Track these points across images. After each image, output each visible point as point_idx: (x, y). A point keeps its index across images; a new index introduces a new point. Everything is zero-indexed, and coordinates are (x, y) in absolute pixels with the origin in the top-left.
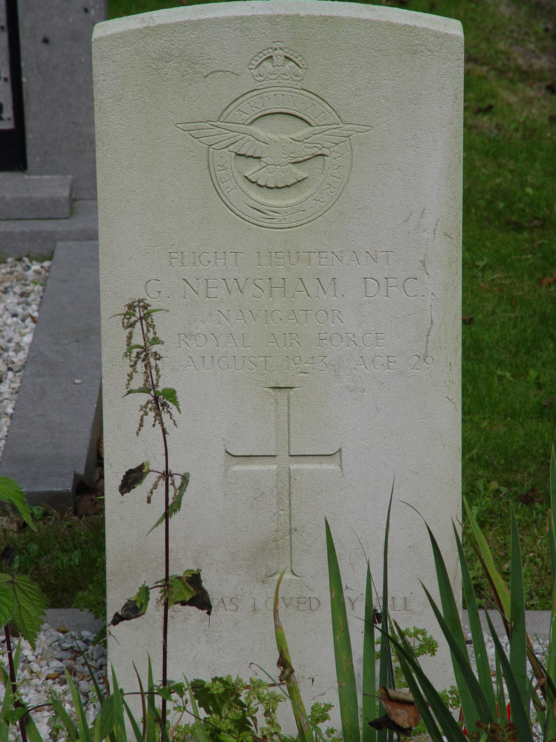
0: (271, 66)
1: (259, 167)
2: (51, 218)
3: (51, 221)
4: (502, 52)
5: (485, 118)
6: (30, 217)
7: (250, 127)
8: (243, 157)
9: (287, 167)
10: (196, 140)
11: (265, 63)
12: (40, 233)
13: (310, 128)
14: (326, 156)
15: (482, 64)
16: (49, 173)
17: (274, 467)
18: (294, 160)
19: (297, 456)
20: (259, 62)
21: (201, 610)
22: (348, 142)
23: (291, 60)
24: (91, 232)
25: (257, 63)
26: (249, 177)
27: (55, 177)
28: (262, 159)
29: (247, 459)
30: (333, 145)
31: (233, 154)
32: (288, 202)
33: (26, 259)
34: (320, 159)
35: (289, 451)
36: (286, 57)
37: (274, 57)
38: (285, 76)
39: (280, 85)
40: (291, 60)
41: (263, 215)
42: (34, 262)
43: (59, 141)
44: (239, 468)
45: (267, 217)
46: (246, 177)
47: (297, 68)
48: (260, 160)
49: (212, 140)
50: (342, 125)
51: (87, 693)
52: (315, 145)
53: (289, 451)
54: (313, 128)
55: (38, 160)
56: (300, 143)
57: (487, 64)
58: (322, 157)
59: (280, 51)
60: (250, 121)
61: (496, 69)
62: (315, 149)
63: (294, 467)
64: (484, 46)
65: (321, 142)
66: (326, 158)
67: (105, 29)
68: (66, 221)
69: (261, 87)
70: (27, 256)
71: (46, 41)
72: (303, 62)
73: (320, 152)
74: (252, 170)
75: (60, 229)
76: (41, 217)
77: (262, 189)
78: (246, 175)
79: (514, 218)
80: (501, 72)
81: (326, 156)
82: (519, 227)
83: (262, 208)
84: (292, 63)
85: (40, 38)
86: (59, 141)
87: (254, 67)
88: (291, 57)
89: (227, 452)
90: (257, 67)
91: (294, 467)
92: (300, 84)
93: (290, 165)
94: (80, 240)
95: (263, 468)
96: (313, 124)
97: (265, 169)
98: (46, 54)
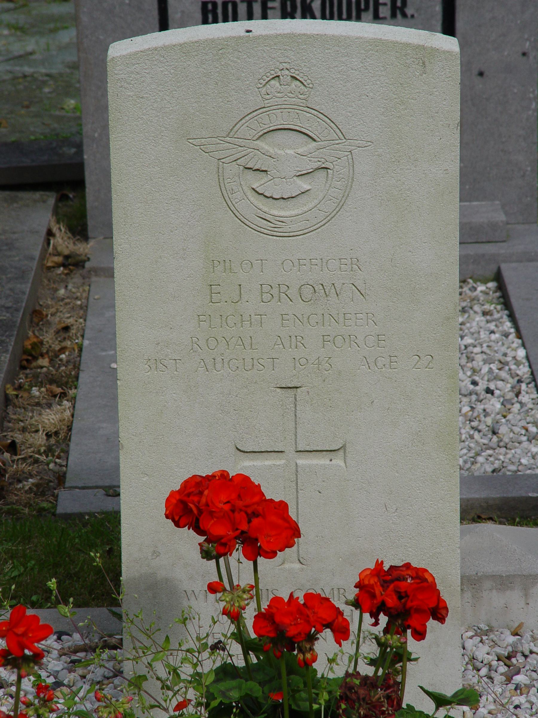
2: (489, 242)
3: (490, 244)
6: (470, 241)
7: (258, 142)
8: (258, 172)
9: (292, 180)
10: (207, 154)
11: (273, 82)
12: (484, 255)
13: (314, 144)
14: (329, 169)
16: (477, 200)
19: (302, 451)
20: (267, 81)
21: (341, 609)
22: (350, 157)
23: (297, 79)
24: (533, 254)
27: (483, 203)
28: (268, 173)
30: (337, 159)
31: (242, 168)
32: (293, 213)
33: (470, 281)
34: (323, 173)
35: (296, 448)
37: (281, 77)
40: (297, 79)
42: (479, 283)
43: (488, 169)
46: (253, 189)
47: (303, 87)
49: (221, 154)
52: (319, 159)
53: (296, 448)
54: (317, 143)
55: (467, 187)
59: (287, 72)
60: (257, 136)
62: (318, 163)
63: (300, 462)
65: (323, 156)
68: (504, 244)
69: (268, 105)
70: (471, 278)
71: (481, 74)
72: (309, 81)
73: (323, 166)
74: (257, 182)
75: (502, 251)
76: (479, 240)
77: (268, 200)
78: (254, 187)
81: (329, 169)
83: (268, 217)
84: (298, 83)
85: (475, 72)
86: (488, 169)
87: (262, 86)
88: (298, 77)
89: (237, 448)
90: (264, 86)
91: (300, 462)
94: (521, 262)
95: (251, 463)
96: (318, 139)
97: (272, 181)
98: (481, 86)
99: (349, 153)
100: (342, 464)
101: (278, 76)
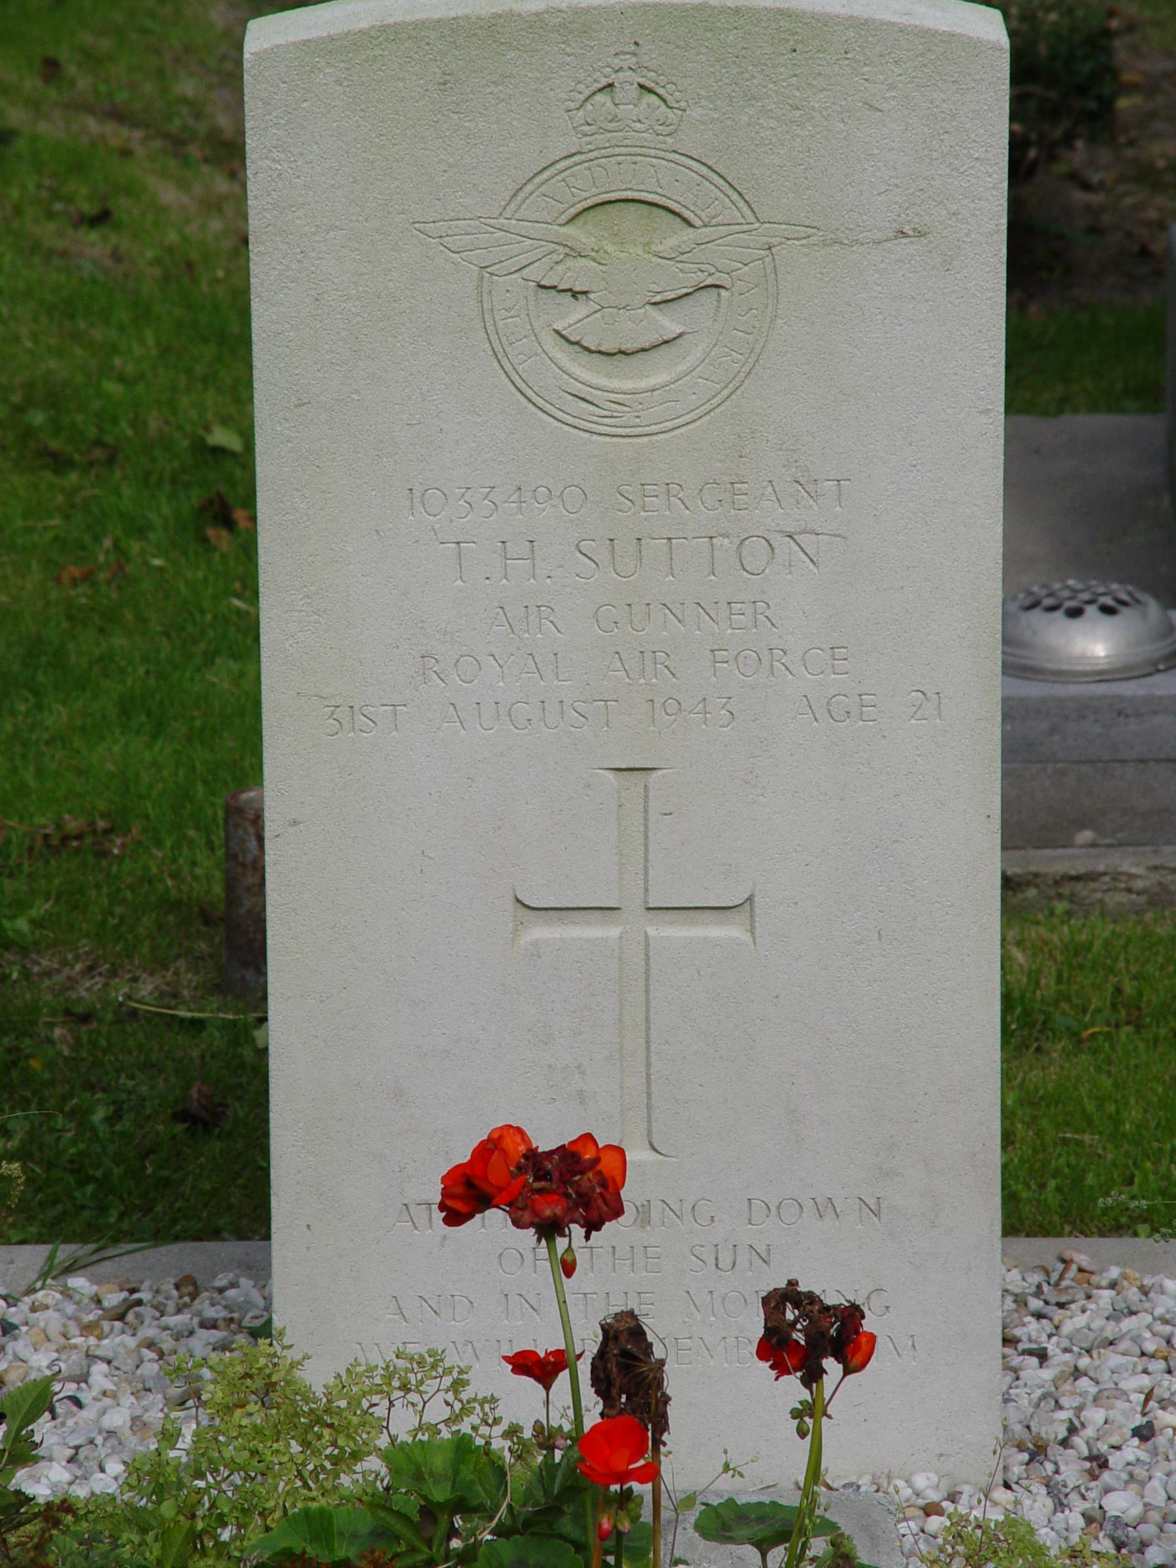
0: (609, 104)
1: (585, 312)
4: (185, 101)
5: (93, 236)
8: (553, 292)
9: (643, 310)
11: (599, 97)
15: (135, 124)
17: (614, 932)
18: (658, 298)
23: (650, 91)
25: (582, 97)
26: (564, 333)
28: (592, 296)
29: (720, 915)
34: (708, 297)
35: (646, 902)
36: (641, 86)
38: (638, 125)
39: (626, 142)
40: (650, 91)
41: (591, 408)
44: (541, 932)
45: (605, 413)
46: (557, 332)
47: (663, 108)
48: (588, 299)
50: (757, 225)
51: (86, 1382)
56: (672, 263)
57: (147, 126)
58: (715, 290)
61: (167, 136)
64: (149, 87)
66: (723, 293)
67: (264, 35)
73: (709, 281)
78: (559, 328)
79: (54, 445)
80: (177, 143)
82: (59, 463)
84: (653, 98)
89: (518, 901)
92: (669, 140)
93: (648, 307)
96: (698, 223)
97: (598, 315)
99: (767, 252)
100: (746, 937)
101: (611, 85)
